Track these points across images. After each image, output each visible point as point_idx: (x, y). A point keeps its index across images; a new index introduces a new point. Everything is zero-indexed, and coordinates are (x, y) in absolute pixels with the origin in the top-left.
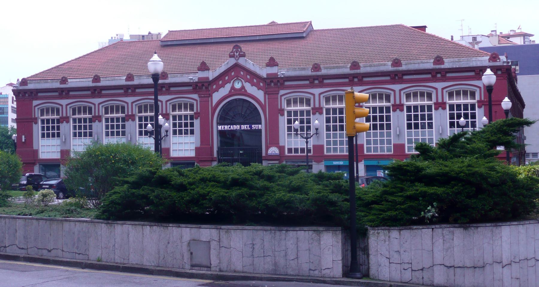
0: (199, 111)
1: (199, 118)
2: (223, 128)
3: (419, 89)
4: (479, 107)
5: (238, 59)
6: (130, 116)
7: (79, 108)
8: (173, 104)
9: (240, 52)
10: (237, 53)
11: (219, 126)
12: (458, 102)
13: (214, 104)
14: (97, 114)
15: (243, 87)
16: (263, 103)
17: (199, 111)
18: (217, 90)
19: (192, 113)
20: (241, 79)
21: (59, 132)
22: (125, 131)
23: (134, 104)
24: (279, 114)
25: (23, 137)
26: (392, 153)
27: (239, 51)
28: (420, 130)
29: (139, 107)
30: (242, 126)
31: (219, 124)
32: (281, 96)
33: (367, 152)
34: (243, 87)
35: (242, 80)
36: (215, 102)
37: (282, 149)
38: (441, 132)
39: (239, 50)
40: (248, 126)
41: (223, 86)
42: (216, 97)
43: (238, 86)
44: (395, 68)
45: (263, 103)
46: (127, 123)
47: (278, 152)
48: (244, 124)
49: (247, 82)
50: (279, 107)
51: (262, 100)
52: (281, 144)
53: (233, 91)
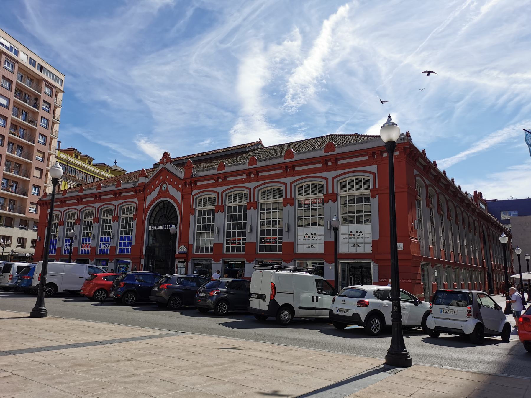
0: (377, 187)
3: (355, 177)
6: (331, 195)
8: (341, 181)
12: (235, 204)
14: (330, 192)
17: (377, 187)
19: (368, 191)
21: (214, 225)
23: (257, 190)
30: (165, 226)
31: (150, 224)
33: (260, 252)
37: (190, 247)
42: (149, 199)
44: (326, 154)
47: (186, 250)
48: (166, 225)
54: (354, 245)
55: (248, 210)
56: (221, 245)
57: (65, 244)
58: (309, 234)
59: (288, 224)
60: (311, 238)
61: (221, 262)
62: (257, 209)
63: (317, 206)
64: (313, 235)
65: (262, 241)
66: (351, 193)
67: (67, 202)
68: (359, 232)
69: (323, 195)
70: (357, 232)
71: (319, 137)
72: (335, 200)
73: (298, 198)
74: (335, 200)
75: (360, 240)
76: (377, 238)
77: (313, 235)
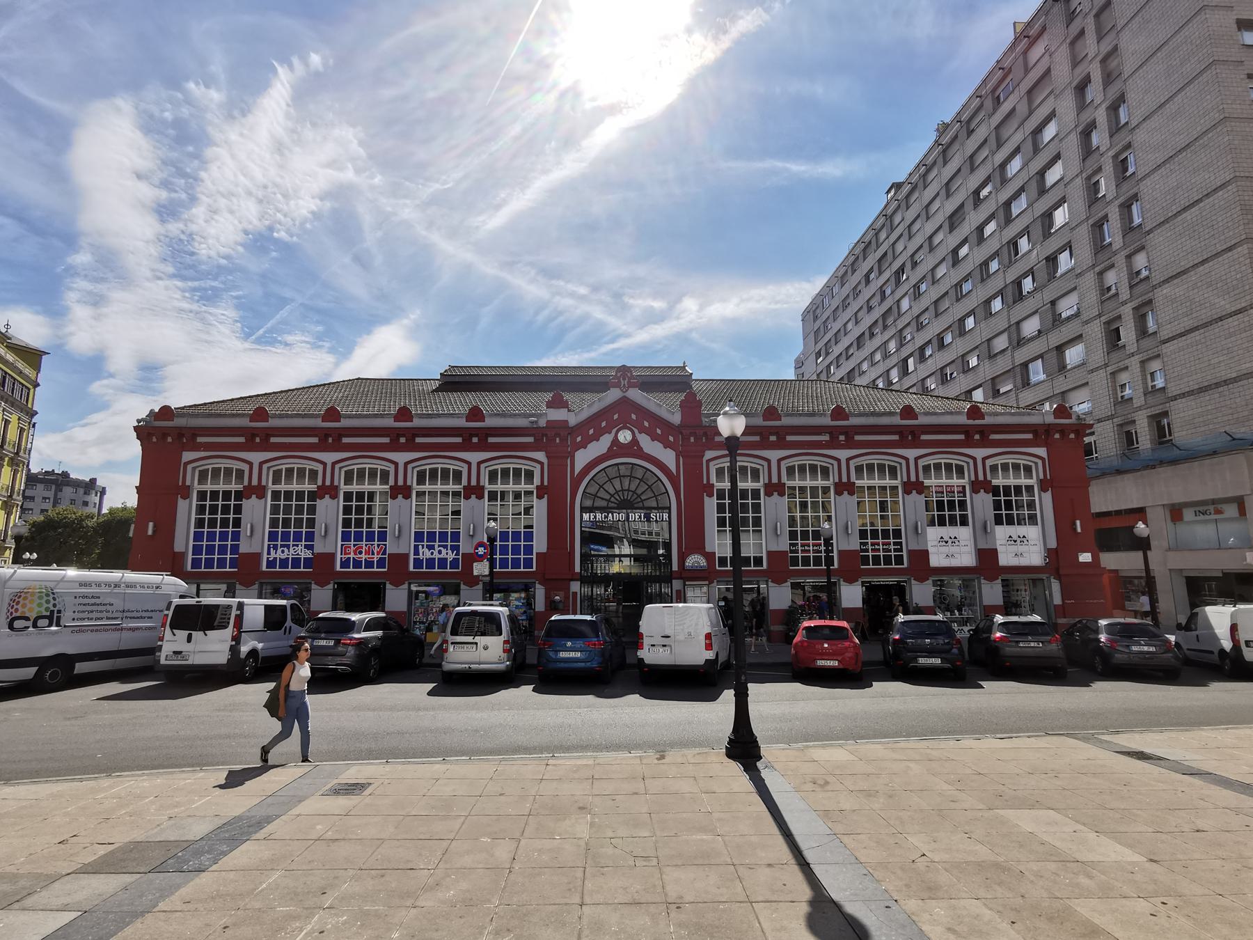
0: (546, 483)
1: (546, 496)
2: (592, 517)
4: (540, 497)
5: (627, 391)
7: (290, 471)
9: (630, 379)
10: (624, 379)
11: (584, 514)
13: (577, 471)
15: (634, 441)
16: (674, 471)
17: (546, 483)
18: (584, 445)
20: (634, 429)
22: (240, 518)
24: (179, 496)
25: (151, 525)
26: (534, 569)
27: (628, 377)
28: (891, 528)
29: (275, 472)
32: (708, 461)
34: (634, 441)
35: (634, 429)
36: (578, 468)
38: (471, 533)
39: (629, 375)
40: (642, 515)
41: (596, 438)
42: (582, 458)
43: (625, 436)
44: (971, 422)
45: (674, 471)
46: (245, 503)
47: (705, 564)
49: (643, 434)
50: (705, 482)
51: (673, 468)
52: (708, 549)
53: (617, 449)
54: (1016, 555)
55: (244, 500)
56: (332, 556)
57: (269, 545)
58: (1015, 538)
59: (326, 525)
60: (1018, 541)
61: (331, 586)
62: (188, 500)
63: (956, 496)
64: (954, 540)
65: (794, 548)
66: (949, 482)
67: (198, 438)
68: (953, 538)
69: (242, 486)
70: (1019, 537)
71: (250, 397)
72: (407, 496)
73: (790, 483)
74: (407, 496)
75: (1021, 549)
76: (1053, 544)
77: (954, 540)
